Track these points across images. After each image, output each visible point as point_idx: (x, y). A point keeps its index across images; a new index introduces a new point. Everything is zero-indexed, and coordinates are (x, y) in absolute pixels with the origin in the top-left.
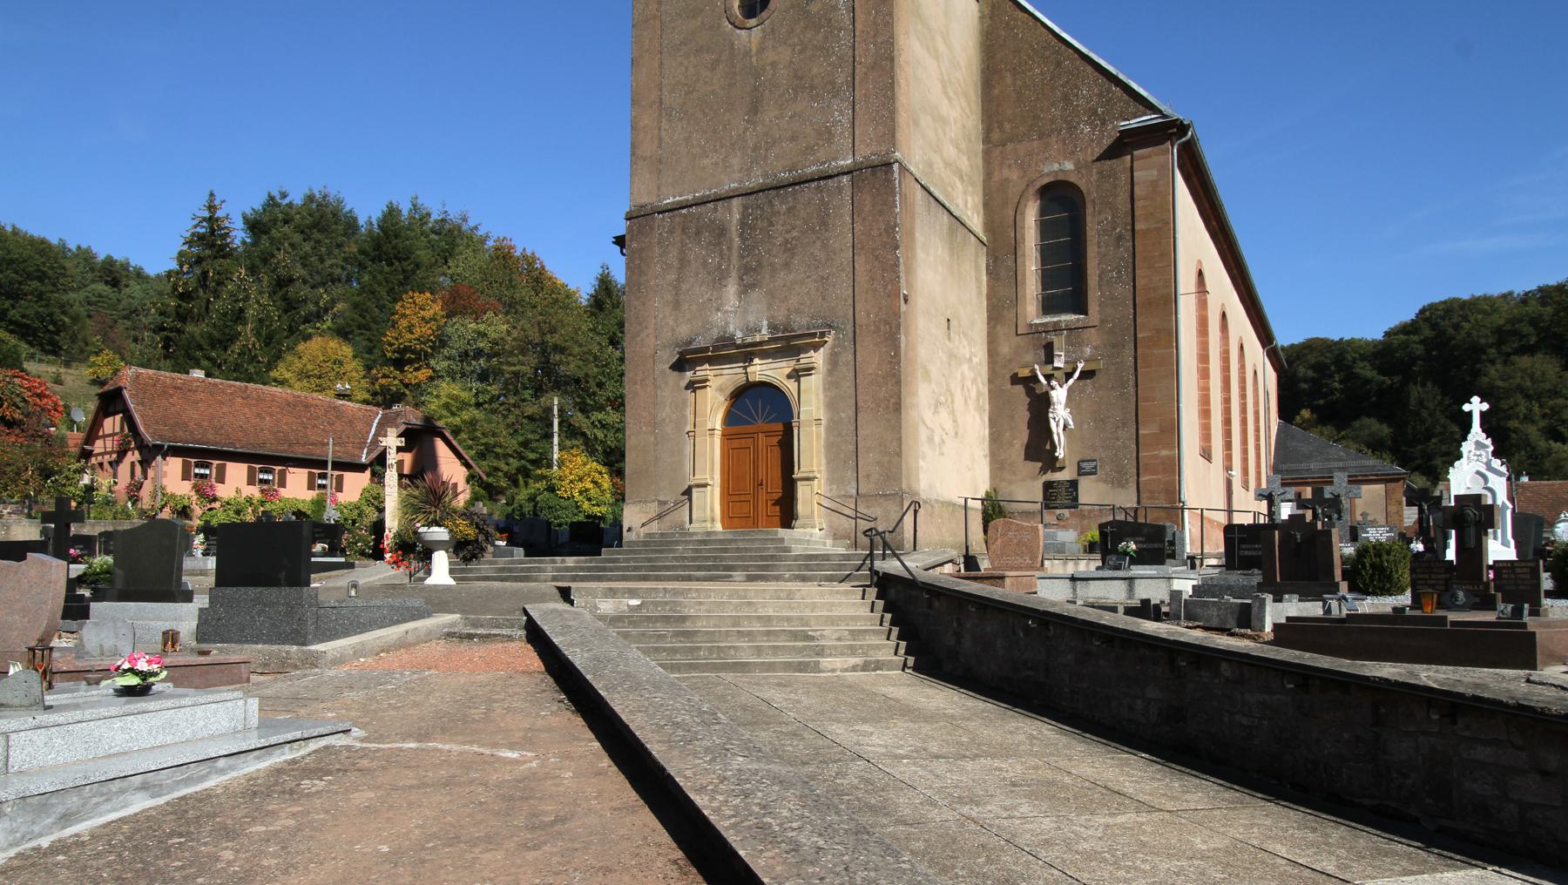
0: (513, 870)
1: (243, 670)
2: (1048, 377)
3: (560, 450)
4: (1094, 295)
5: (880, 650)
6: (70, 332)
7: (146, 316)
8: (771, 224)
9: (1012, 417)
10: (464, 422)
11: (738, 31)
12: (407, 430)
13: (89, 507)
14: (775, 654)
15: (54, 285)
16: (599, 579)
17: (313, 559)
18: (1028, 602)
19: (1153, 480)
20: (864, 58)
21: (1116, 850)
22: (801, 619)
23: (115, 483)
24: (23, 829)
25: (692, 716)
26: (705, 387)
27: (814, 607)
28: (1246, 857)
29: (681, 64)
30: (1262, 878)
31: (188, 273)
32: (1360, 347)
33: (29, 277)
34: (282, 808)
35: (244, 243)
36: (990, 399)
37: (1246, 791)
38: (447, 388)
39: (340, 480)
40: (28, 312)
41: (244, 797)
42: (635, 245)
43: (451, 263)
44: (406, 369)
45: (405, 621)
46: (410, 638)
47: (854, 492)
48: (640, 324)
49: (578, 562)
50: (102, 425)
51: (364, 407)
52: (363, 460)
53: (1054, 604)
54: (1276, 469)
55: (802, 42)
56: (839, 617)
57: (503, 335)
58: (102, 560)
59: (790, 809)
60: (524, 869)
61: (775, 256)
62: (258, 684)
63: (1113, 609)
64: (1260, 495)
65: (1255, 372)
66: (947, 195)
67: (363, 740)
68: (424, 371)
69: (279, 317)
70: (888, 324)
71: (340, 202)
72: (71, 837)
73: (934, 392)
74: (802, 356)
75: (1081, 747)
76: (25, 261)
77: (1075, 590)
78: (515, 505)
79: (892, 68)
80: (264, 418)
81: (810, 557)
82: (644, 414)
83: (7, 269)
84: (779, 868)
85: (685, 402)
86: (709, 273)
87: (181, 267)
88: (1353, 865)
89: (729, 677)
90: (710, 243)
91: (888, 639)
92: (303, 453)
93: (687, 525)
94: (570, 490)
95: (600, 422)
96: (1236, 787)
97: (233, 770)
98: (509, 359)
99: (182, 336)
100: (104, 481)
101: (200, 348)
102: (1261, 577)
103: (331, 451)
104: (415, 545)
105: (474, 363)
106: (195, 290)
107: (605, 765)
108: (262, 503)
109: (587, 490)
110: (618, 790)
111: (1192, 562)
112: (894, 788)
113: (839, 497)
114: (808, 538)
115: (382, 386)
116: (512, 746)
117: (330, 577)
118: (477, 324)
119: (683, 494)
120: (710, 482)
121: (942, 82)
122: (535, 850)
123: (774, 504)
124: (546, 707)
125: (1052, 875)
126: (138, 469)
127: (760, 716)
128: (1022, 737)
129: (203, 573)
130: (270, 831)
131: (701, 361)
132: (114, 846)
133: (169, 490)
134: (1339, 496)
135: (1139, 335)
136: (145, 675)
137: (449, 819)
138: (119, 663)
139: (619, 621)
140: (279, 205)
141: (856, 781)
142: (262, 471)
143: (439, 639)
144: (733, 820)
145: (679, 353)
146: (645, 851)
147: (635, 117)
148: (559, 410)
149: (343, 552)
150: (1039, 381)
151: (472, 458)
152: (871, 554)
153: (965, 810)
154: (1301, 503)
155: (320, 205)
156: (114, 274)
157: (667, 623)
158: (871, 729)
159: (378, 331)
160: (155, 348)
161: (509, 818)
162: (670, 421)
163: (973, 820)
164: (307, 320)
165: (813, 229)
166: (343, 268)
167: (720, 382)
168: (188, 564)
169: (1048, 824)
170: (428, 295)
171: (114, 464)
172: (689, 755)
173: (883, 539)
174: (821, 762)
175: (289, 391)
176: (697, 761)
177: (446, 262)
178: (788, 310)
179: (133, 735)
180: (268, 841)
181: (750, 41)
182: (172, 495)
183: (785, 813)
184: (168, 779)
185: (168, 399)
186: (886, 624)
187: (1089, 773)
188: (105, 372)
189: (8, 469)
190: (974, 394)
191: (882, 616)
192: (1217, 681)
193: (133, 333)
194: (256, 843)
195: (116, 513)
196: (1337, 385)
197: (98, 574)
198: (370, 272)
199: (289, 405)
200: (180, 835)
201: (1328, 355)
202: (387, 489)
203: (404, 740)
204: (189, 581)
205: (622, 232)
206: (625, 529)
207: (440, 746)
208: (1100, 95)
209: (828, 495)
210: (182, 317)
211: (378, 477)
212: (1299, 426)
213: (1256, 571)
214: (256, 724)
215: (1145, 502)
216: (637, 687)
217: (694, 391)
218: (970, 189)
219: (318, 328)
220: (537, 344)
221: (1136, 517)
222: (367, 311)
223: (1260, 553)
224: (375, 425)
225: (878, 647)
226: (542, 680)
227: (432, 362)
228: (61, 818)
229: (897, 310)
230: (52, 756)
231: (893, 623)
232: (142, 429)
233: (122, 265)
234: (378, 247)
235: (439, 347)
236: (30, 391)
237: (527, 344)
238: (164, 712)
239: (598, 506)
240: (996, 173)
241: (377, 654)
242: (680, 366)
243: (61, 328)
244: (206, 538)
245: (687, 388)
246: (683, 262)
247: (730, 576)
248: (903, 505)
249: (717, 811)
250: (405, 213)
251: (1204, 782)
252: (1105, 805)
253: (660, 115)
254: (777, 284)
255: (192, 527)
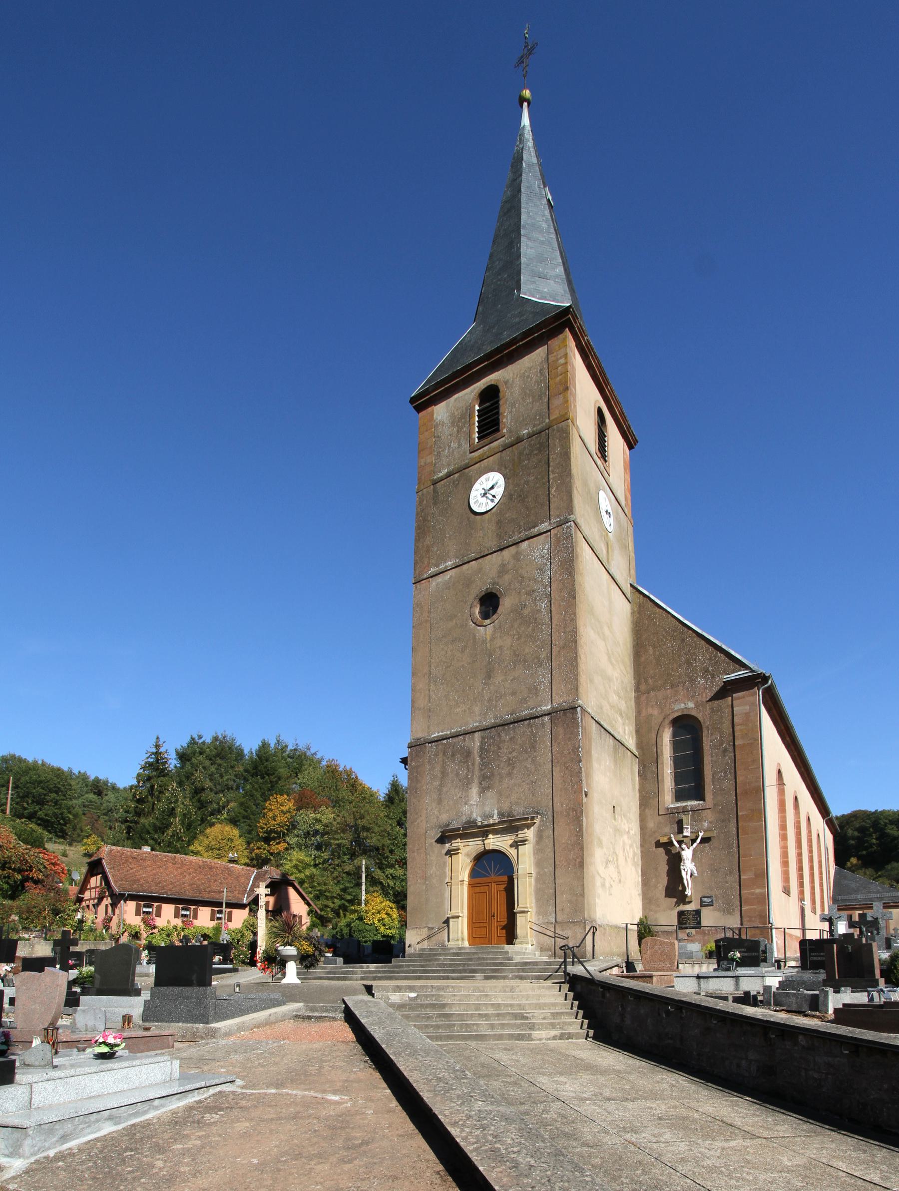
0: (335, 1177)
1: (170, 1040)
2: (680, 842)
3: (366, 894)
4: (709, 788)
5: (571, 1025)
6: (73, 824)
7: (117, 813)
8: (500, 748)
9: (656, 869)
10: (306, 876)
11: (479, 628)
12: (271, 882)
13: (80, 933)
14: (503, 1029)
15: (64, 795)
16: (390, 978)
17: (214, 966)
18: (668, 994)
19: (751, 909)
20: (558, 641)
21: (729, 1165)
22: (519, 1005)
23: (96, 918)
24: (39, 1145)
25: (449, 1073)
26: (458, 853)
27: (528, 997)
28: (818, 1171)
29: (443, 649)
30: (829, 1186)
31: (142, 786)
32: (889, 815)
33: (51, 791)
34: (193, 1133)
35: (176, 767)
36: (641, 858)
37: (818, 1124)
38: (297, 855)
39: (230, 914)
40: (49, 812)
41: (170, 1125)
42: (413, 764)
43: (300, 776)
44: (271, 843)
45: (269, 1008)
46: (272, 1018)
47: (554, 920)
48: (417, 814)
49: (377, 967)
50: (90, 882)
51: (245, 868)
52: (245, 902)
53: (685, 995)
54: (835, 900)
55: (519, 633)
56: (545, 1004)
57: (331, 821)
58: (87, 969)
59: (512, 1138)
60: (342, 1176)
61: (503, 769)
62: (178, 1049)
63: (725, 999)
64: (823, 919)
65: (818, 835)
66: (613, 727)
67: (243, 1087)
68: (282, 844)
69: (195, 812)
70: (575, 811)
71: (233, 740)
72: (66, 1150)
73: (605, 854)
74: (519, 832)
75: (705, 1093)
76: (48, 781)
77: (699, 985)
78: (338, 929)
79: (576, 648)
80: (185, 876)
81: (526, 964)
82: (419, 871)
83: (38, 786)
84: (505, 1180)
85: (445, 863)
86: (460, 780)
87: (139, 783)
88: (892, 1177)
89: (473, 1044)
90: (461, 762)
91: (576, 1018)
92: (208, 898)
93: (446, 943)
94: (373, 919)
95: (391, 875)
96: (810, 1121)
97: (164, 1107)
98: (335, 836)
99: (138, 825)
100: (89, 916)
101: (148, 833)
102: (825, 975)
103: (225, 896)
104: (275, 958)
105: (313, 838)
106: (146, 796)
107: (394, 1105)
108: (183, 929)
109: (383, 919)
110: (401, 1122)
111: (778, 964)
112: (581, 1121)
113: (544, 924)
114: (524, 951)
115: (256, 854)
116: (335, 1092)
117: (223, 978)
118: (315, 814)
119: (444, 923)
120: (461, 915)
121: (608, 654)
122: (349, 1163)
123: (502, 929)
124: (356, 1066)
125: (686, 1183)
126: (110, 908)
127: (492, 1071)
128: (665, 1086)
129: (147, 975)
130: (186, 1148)
131: (455, 837)
132: (91, 1157)
133: (127, 922)
134: (877, 919)
135: (740, 814)
136: (112, 1046)
137: (296, 1141)
138: (97, 1038)
139: (403, 1007)
140: (197, 743)
141: (556, 1116)
142: (183, 909)
143: (290, 1019)
144: (475, 1146)
145: (441, 832)
146: (419, 1165)
147: (414, 684)
148: (366, 868)
149: (231, 961)
150: (674, 845)
151: (311, 899)
152: (565, 962)
153: (628, 1136)
154: (851, 925)
155: (221, 742)
156: (99, 788)
157: (434, 1008)
158: (565, 1080)
159: (255, 820)
160: (122, 833)
161: (332, 1142)
162: (436, 876)
163: (633, 1144)
164: (212, 814)
165: (526, 752)
166: (234, 781)
167: (468, 849)
168: (138, 969)
169: (683, 1146)
170: (285, 796)
171: (96, 906)
172: (447, 1100)
173: (573, 952)
174: (533, 1102)
175: (200, 859)
176: (453, 1105)
177: (297, 775)
178: (510, 803)
179: (104, 1084)
180: (184, 1155)
181: (486, 634)
182: (129, 925)
183: (509, 1141)
184: (125, 1112)
185: (128, 865)
186: (575, 1008)
187: (711, 1111)
188: (93, 849)
189: (34, 910)
190: (631, 855)
191: (572, 1003)
192: (796, 1048)
193: (109, 823)
194: (177, 1156)
195: (96, 937)
196: (874, 841)
197: (85, 978)
198: (251, 783)
199: (200, 867)
200: (131, 1150)
201: (868, 821)
202: (259, 921)
203: (268, 1088)
204: (139, 982)
205: (406, 755)
206: (407, 945)
207: (290, 1092)
208: (710, 659)
209: (537, 923)
210: (138, 814)
211: (253, 912)
212: (849, 869)
213: (822, 971)
214: (178, 1077)
215: (746, 924)
216: (414, 1053)
217: (451, 856)
218: (627, 721)
219: (219, 819)
220: (352, 826)
221: (740, 935)
222: (248, 808)
223: (824, 959)
224: (252, 879)
225: (570, 1024)
226: (354, 1047)
227: (288, 839)
228: (61, 1138)
229: (581, 802)
230: (57, 1098)
231: (579, 1008)
232: (113, 884)
233: (104, 782)
234: (255, 767)
235: (292, 829)
236: (48, 861)
237: (346, 826)
238: (123, 1070)
239: (390, 929)
240: (644, 711)
241: (252, 1029)
242: (442, 840)
243: (68, 822)
244: (149, 953)
245: (446, 854)
246: (444, 773)
247: (474, 976)
248: (585, 928)
249: (465, 1139)
250: (272, 745)
251: (789, 1117)
252: (721, 1133)
253: (430, 681)
254: (503, 786)
255: (140, 945)
